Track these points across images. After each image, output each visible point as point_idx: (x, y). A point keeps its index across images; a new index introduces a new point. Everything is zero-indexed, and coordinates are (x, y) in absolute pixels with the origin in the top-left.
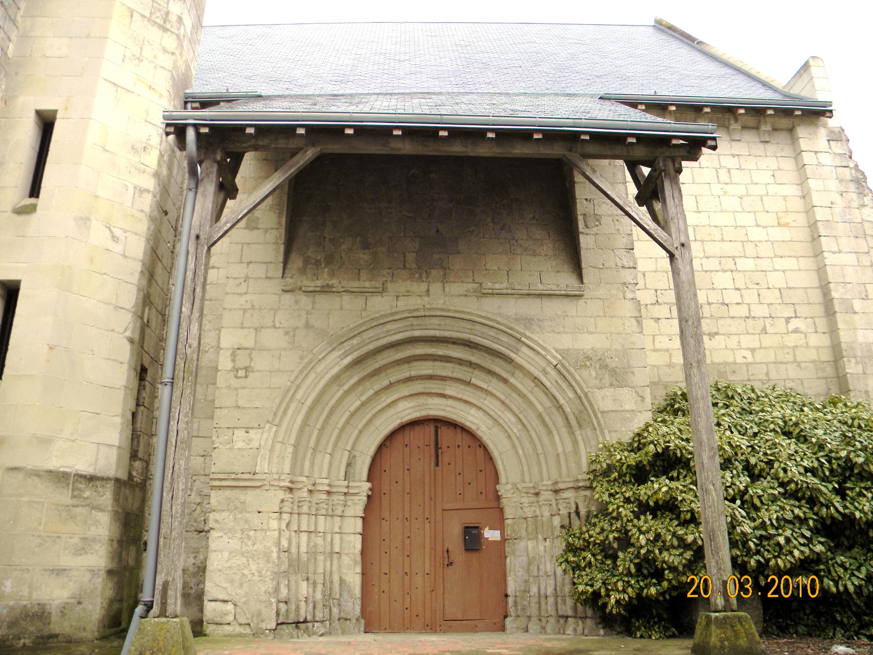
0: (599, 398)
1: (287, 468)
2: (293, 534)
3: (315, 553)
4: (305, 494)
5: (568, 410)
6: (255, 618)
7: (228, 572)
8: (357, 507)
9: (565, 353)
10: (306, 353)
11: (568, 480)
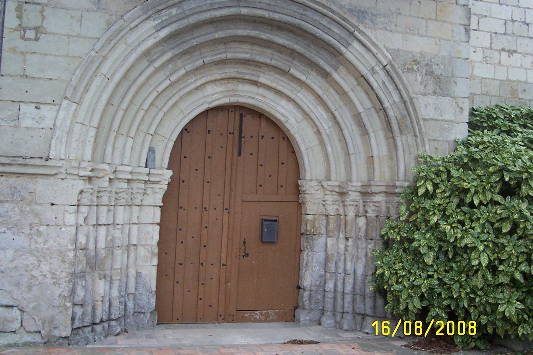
0: (422, 104)
1: (88, 155)
2: (91, 228)
3: (113, 247)
4: (106, 184)
5: (391, 113)
6: (46, 325)
7: (12, 274)
8: (156, 197)
9: (395, 53)
10: (114, 18)
11: (381, 184)
